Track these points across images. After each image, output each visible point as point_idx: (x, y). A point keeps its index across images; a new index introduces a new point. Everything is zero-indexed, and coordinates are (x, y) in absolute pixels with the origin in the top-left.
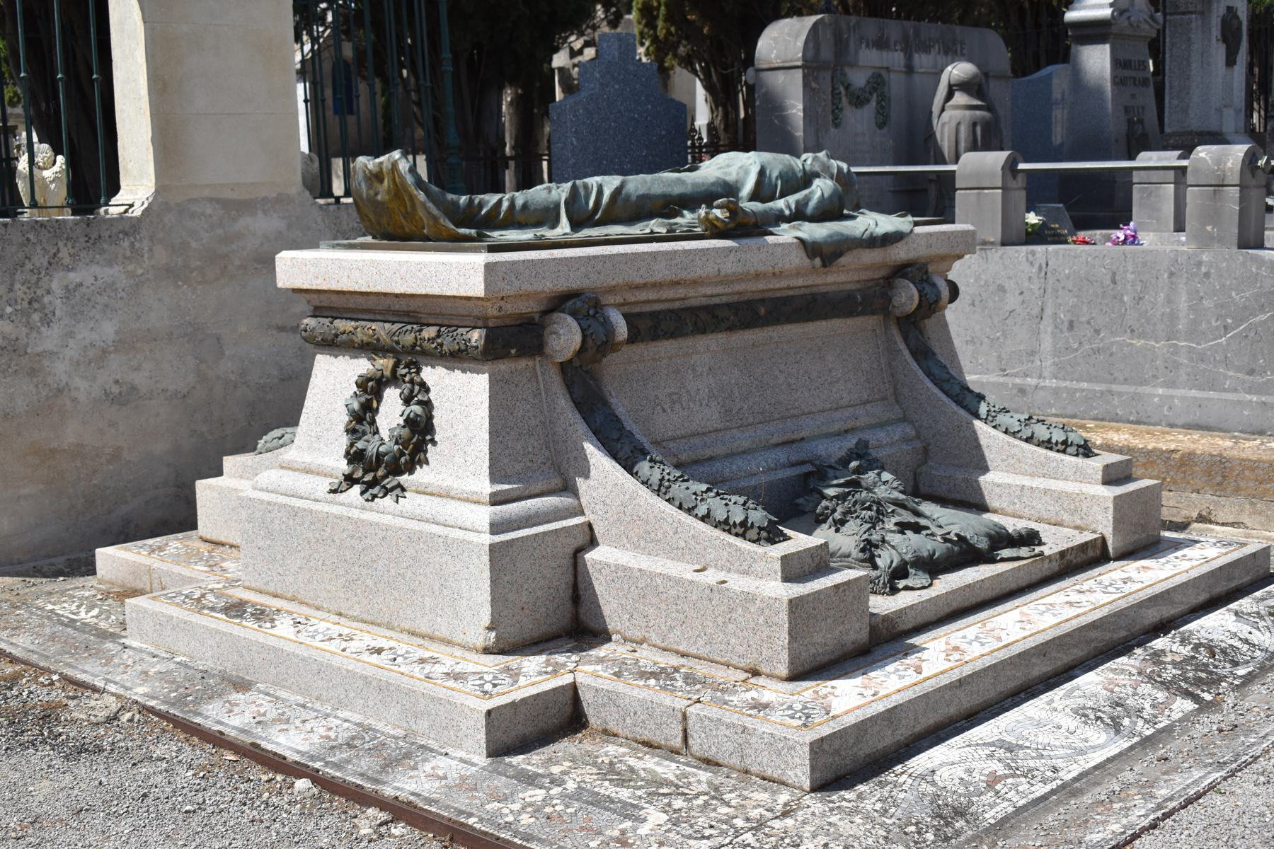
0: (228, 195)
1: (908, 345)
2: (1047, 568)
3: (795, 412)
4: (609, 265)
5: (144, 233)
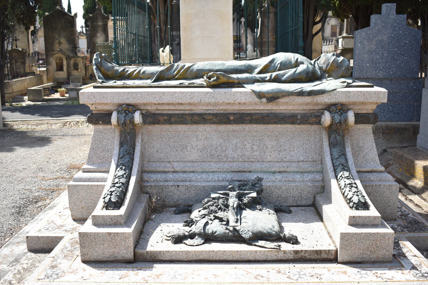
2: (280, 256)
3: (253, 160)
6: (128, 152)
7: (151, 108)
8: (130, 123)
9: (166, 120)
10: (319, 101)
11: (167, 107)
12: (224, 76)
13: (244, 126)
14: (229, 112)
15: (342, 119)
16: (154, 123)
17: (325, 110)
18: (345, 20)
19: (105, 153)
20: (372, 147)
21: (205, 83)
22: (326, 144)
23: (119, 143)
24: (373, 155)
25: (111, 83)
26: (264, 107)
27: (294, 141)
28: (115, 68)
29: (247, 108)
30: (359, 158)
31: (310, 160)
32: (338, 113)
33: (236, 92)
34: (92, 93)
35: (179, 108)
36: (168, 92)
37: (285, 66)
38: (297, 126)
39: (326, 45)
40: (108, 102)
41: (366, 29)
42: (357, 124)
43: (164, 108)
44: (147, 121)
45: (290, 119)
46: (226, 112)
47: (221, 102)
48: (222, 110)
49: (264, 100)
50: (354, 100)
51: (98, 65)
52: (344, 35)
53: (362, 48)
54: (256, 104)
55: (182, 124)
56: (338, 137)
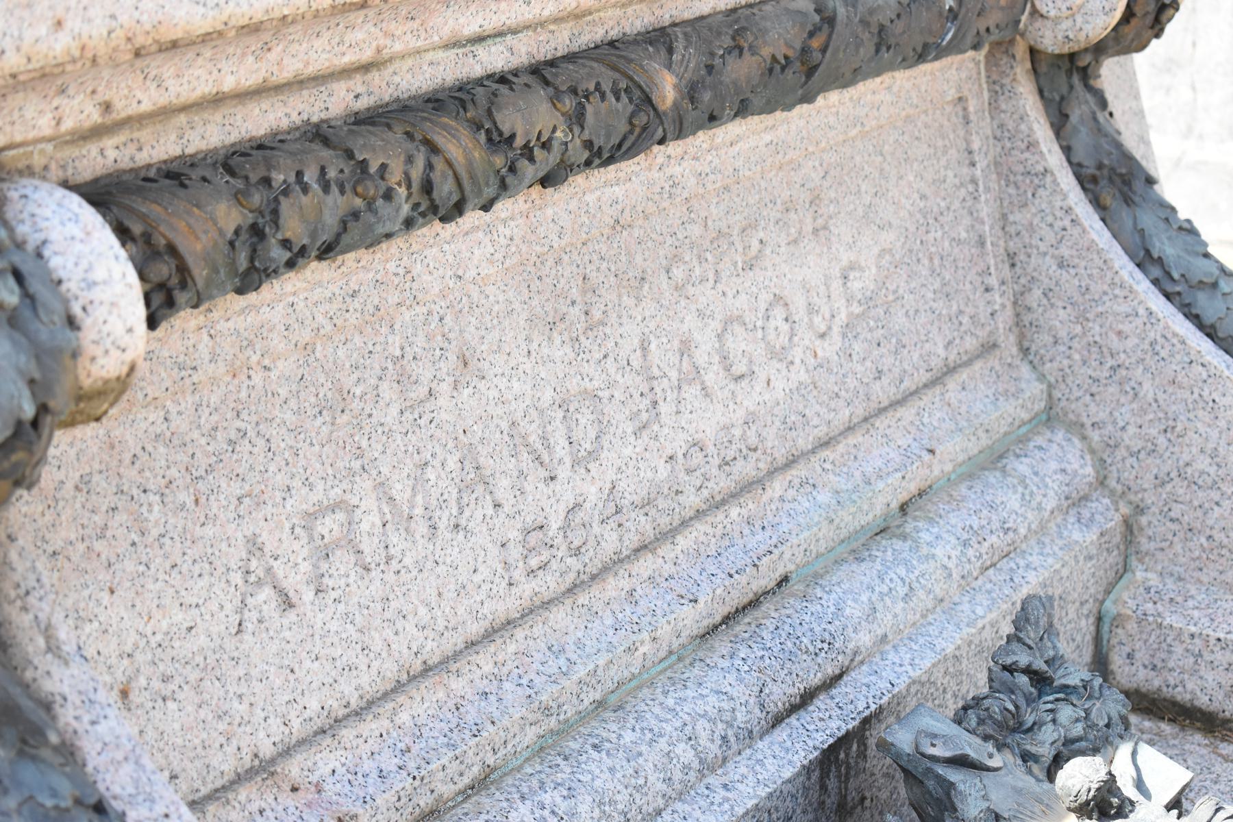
1: (1067, 150)
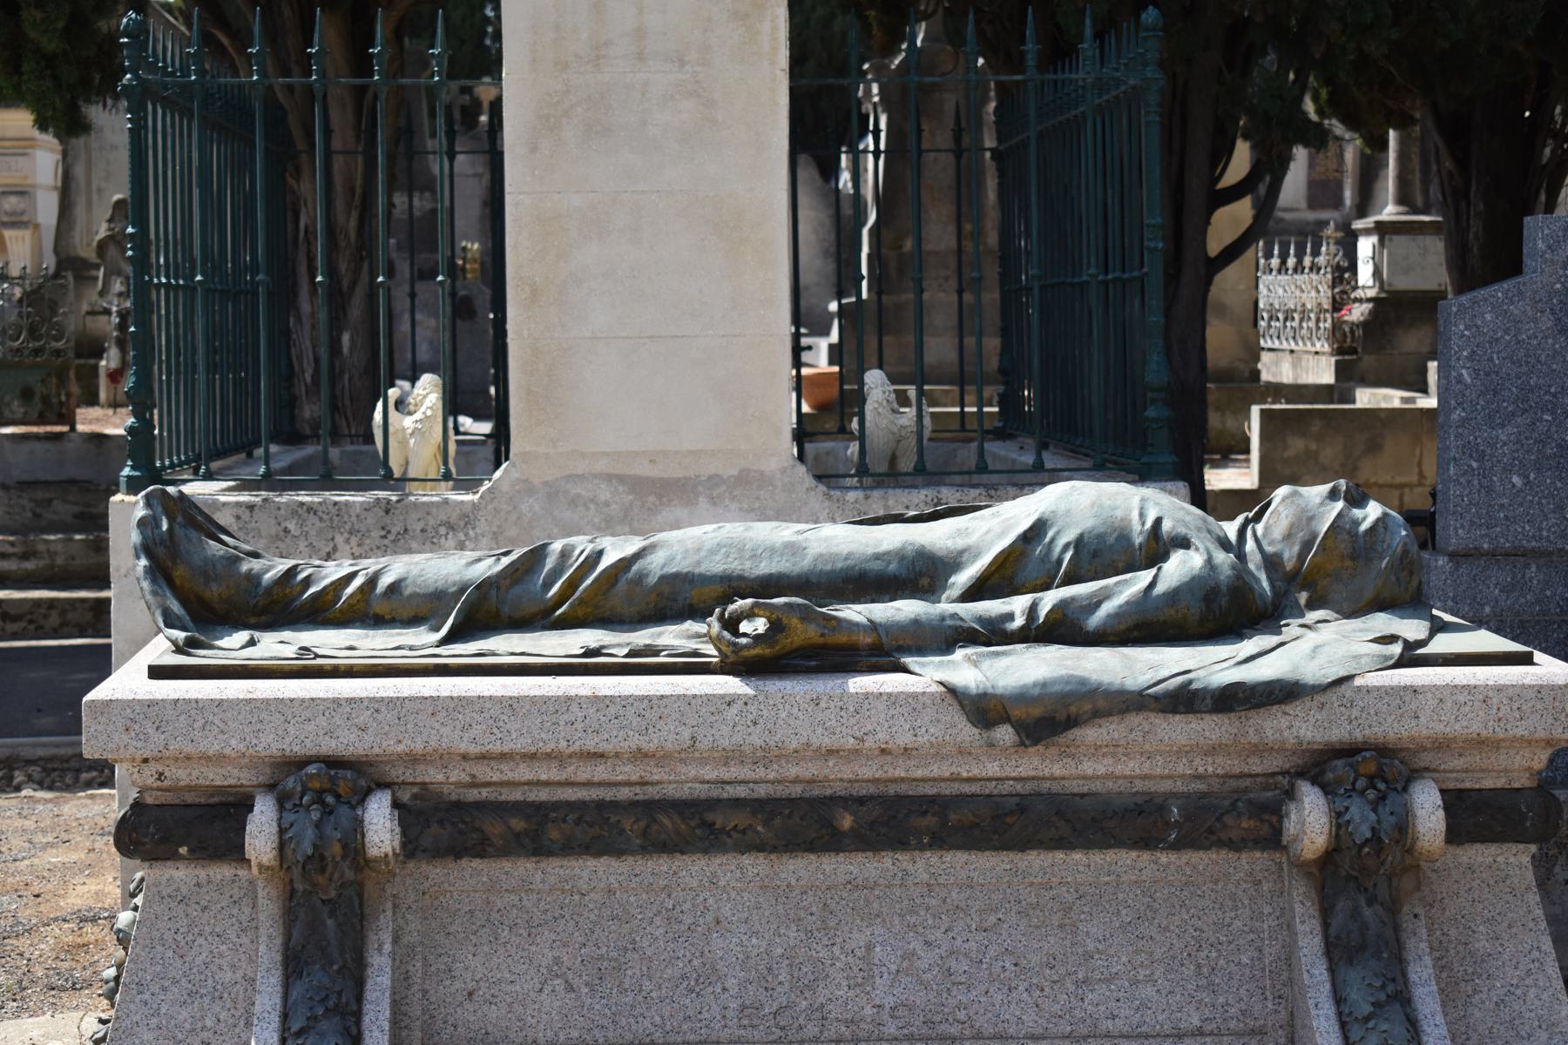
0: (643, 469)
4: (387, 716)
5: (482, 526)
6: (331, 1004)
7: (440, 778)
8: (344, 857)
9: (518, 835)
10: (1270, 735)
11: (524, 772)
12: (806, 615)
13: (903, 858)
14: (829, 792)
15: (1385, 825)
16: (456, 851)
17: (1301, 774)
18: (1392, 135)
19: (202, 1009)
20: (1536, 954)
21: (710, 649)
22: (1310, 944)
23: (279, 957)
24: (1545, 996)
25: (232, 645)
26: (1004, 765)
27: (1153, 931)
28: (244, 567)
29: (919, 773)
30: (1478, 1014)
31: (1233, 1024)
32: (1362, 793)
33: (867, 696)
34: (151, 704)
35: (583, 776)
36: (533, 700)
37: (1103, 554)
38: (1164, 858)
39: (1282, 268)
40: (227, 751)
41: (1498, 291)
42: (1460, 843)
43: (510, 776)
44: (426, 841)
45: (1132, 821)
46: (816, 792)
47: (794, 745)
48: (796, 781)
49: (1005, 734)
50: (1440, 728)
51: (161, 551)
52: (1389, 212)
53: (1482, 394)
54: (962, 752)
55: (598, 854)
56: (1367, 912)
